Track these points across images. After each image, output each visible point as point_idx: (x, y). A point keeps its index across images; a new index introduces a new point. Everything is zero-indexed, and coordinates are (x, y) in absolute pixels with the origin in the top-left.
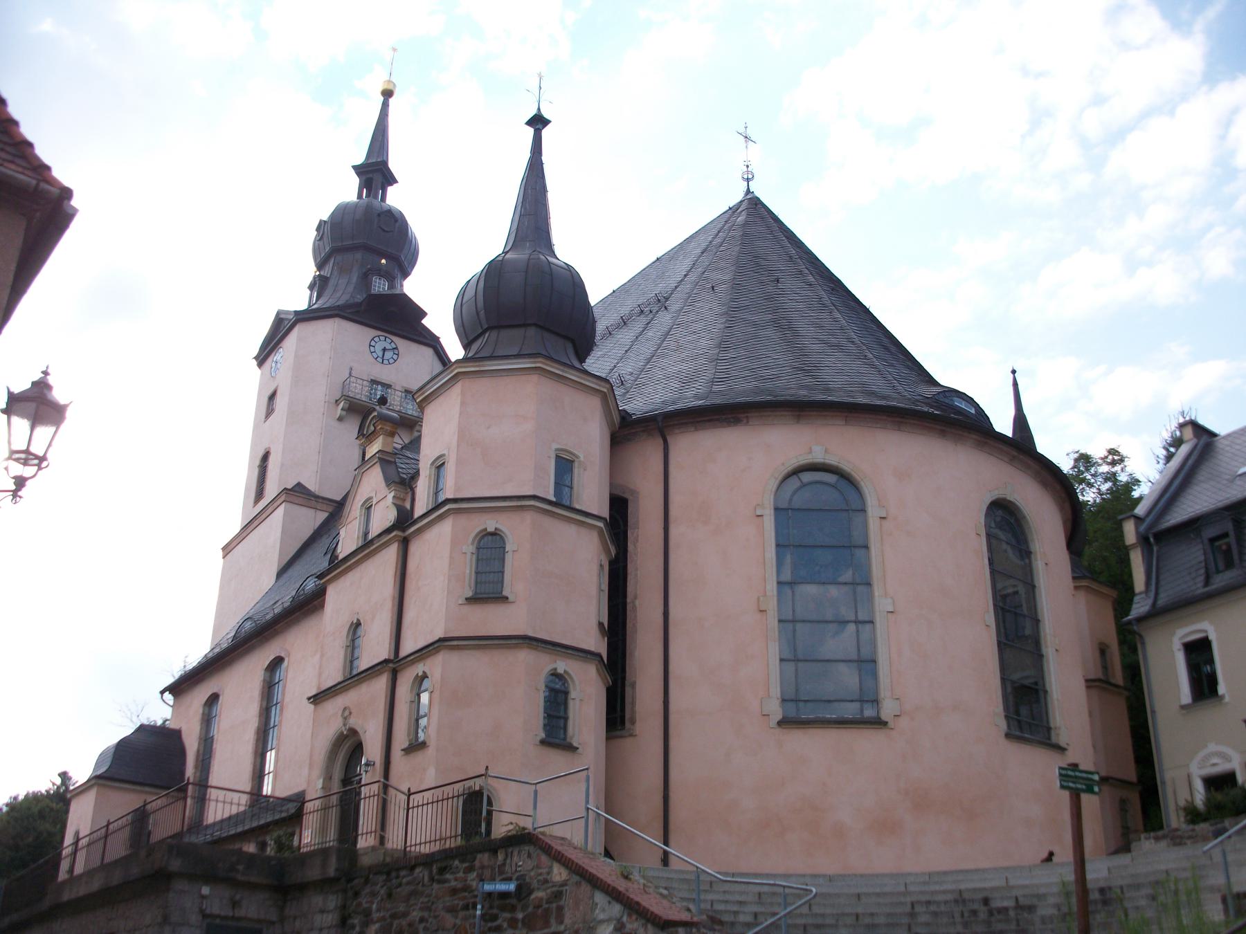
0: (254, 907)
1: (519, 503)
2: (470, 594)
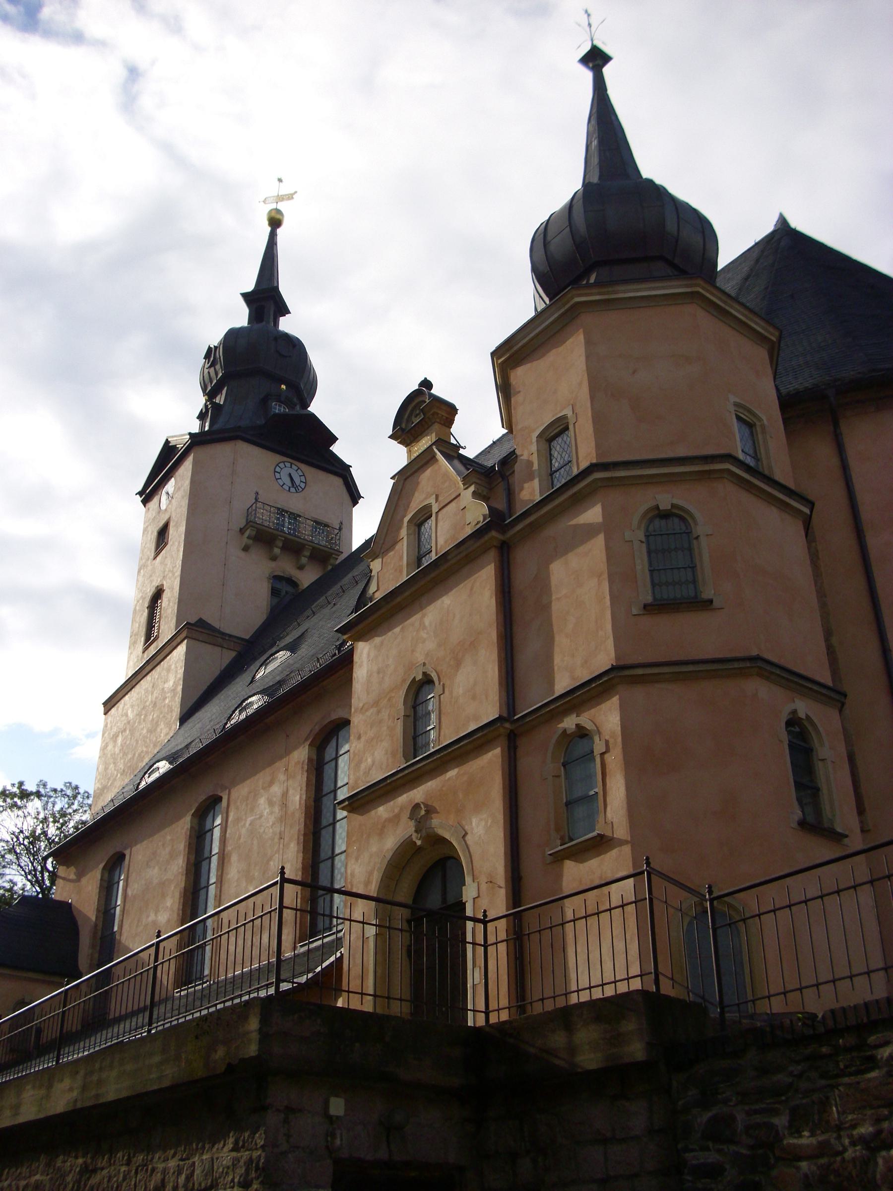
0: (434, 1136)
1: (707, 467)
2: (649, 599)
